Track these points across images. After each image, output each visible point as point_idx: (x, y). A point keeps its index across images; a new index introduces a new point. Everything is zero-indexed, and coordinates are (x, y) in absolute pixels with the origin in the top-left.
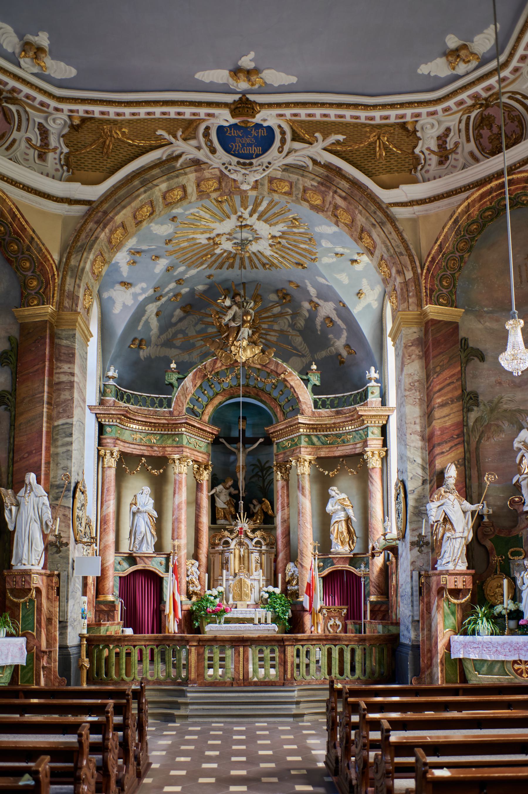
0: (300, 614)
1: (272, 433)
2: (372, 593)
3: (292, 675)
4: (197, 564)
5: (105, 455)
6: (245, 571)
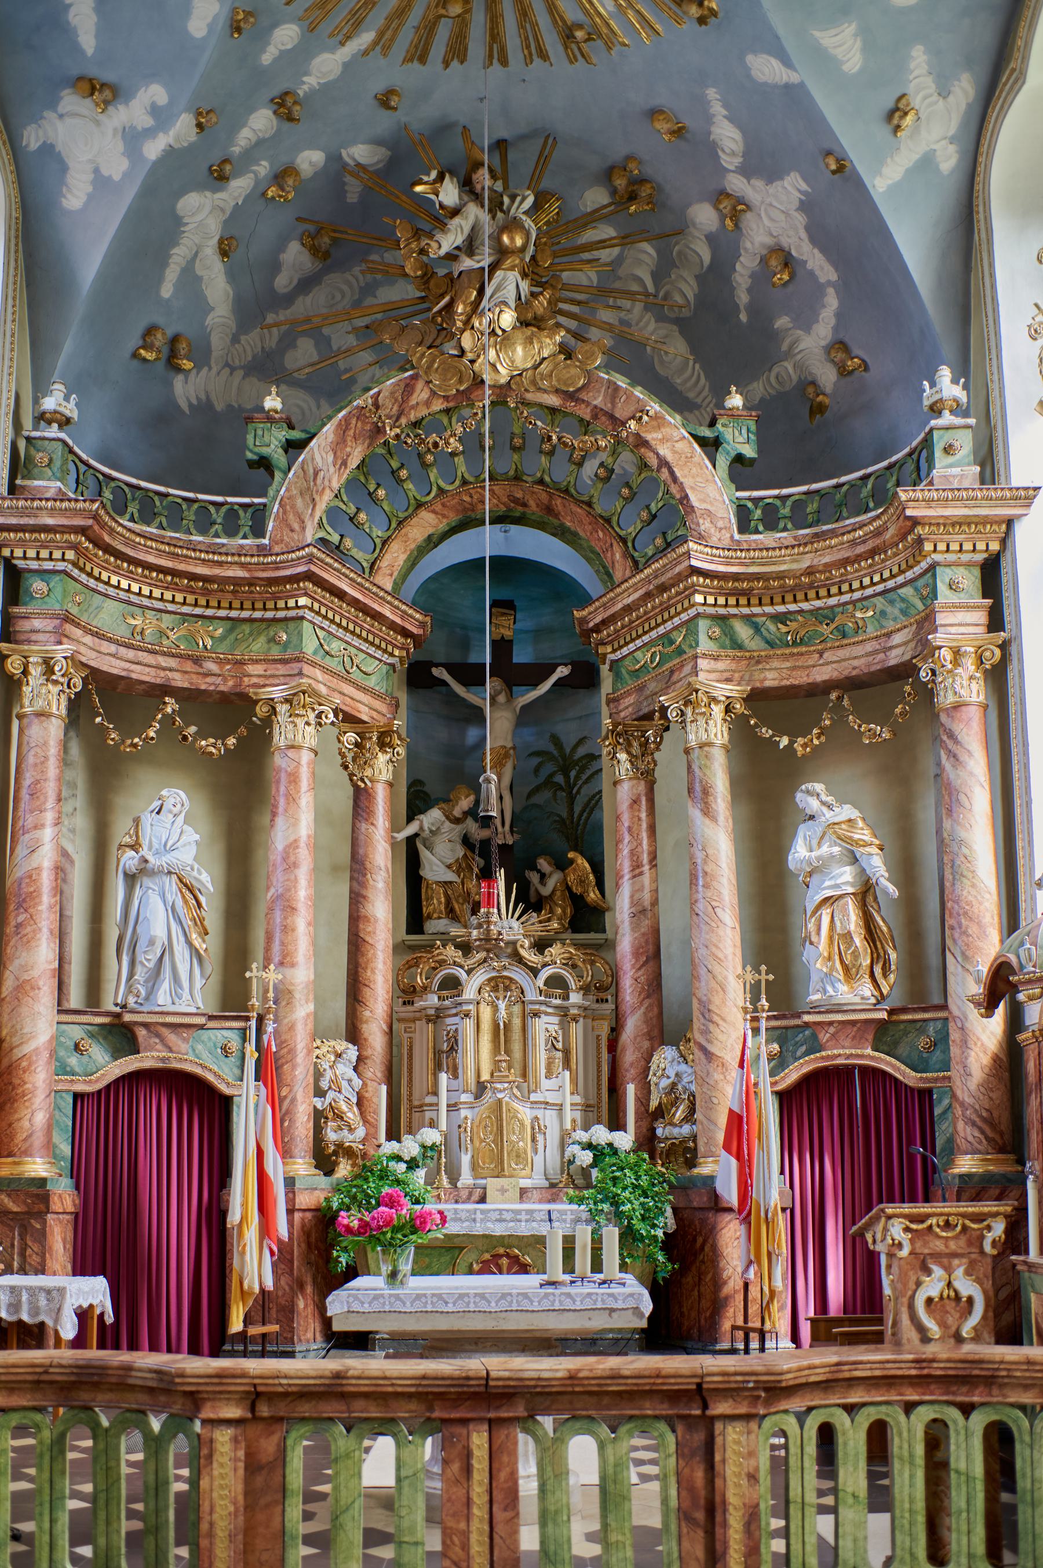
0: (703, 1221)
1: (597, 629)
2: (960, 1141)
4: (352, 1053)
5: (25, 672)
6: (514, 1075)
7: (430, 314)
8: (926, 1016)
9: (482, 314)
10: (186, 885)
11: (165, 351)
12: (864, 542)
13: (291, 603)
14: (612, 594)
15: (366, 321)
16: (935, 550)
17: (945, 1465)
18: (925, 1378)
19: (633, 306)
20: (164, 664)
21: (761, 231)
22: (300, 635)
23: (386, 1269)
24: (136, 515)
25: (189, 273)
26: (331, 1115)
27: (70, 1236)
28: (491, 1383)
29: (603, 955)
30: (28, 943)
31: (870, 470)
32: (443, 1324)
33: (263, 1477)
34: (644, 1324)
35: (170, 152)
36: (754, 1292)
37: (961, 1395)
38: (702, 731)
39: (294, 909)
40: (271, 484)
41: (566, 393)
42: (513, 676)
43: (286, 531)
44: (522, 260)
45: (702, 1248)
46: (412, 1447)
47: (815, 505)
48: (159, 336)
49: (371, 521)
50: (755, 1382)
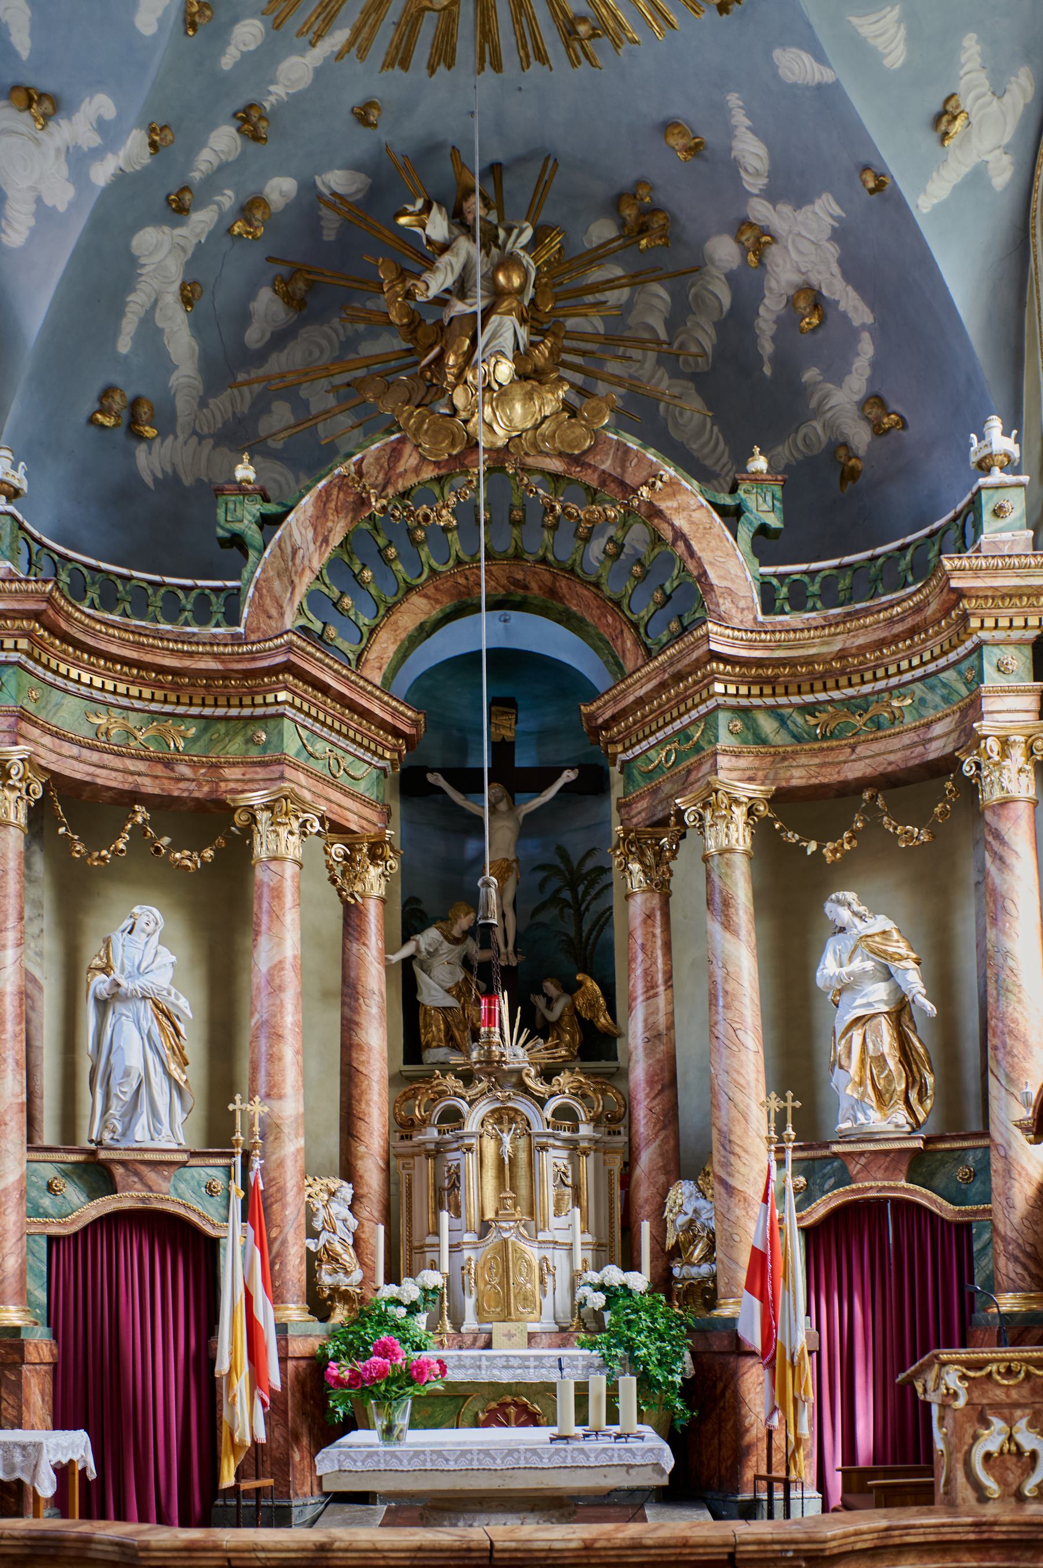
1: (607, 726)
2: (1001, 1278)
7: (418, 368)
8: (966, 1144)
9: (475, 367)
10: (162, 1011)
11: (125, 415)
12: (902, 620)
13: (270, 698)
14: (623, 686)
15: (347, 377)
16: (982, 627)
19: (645, 356)
20: (132, 768)
21: (788, 266)
22: (281, 734)
23: (380, 1423)
24: (97, 601)
25: (148, 323)
26: (325, 1257)
27: (49, 1387)
28: (496, 1555)
29: (615, 1084)
31: (909, 538)
32: (443, 1484)
34: (664, 1481)
35: (121, 177)
36: (778, 1440)
37: (1025, 1561)
38: (722, 836)
39: (280, 1036)
40: (245, 565)
41: (570, 456)
42: (515, 780)
43: (263, 618)
44: (520, 302)
45: (723, 1393)
47: (848, 581)
48: (117, 398)
49: (356, 606)
50: (794, 1551)
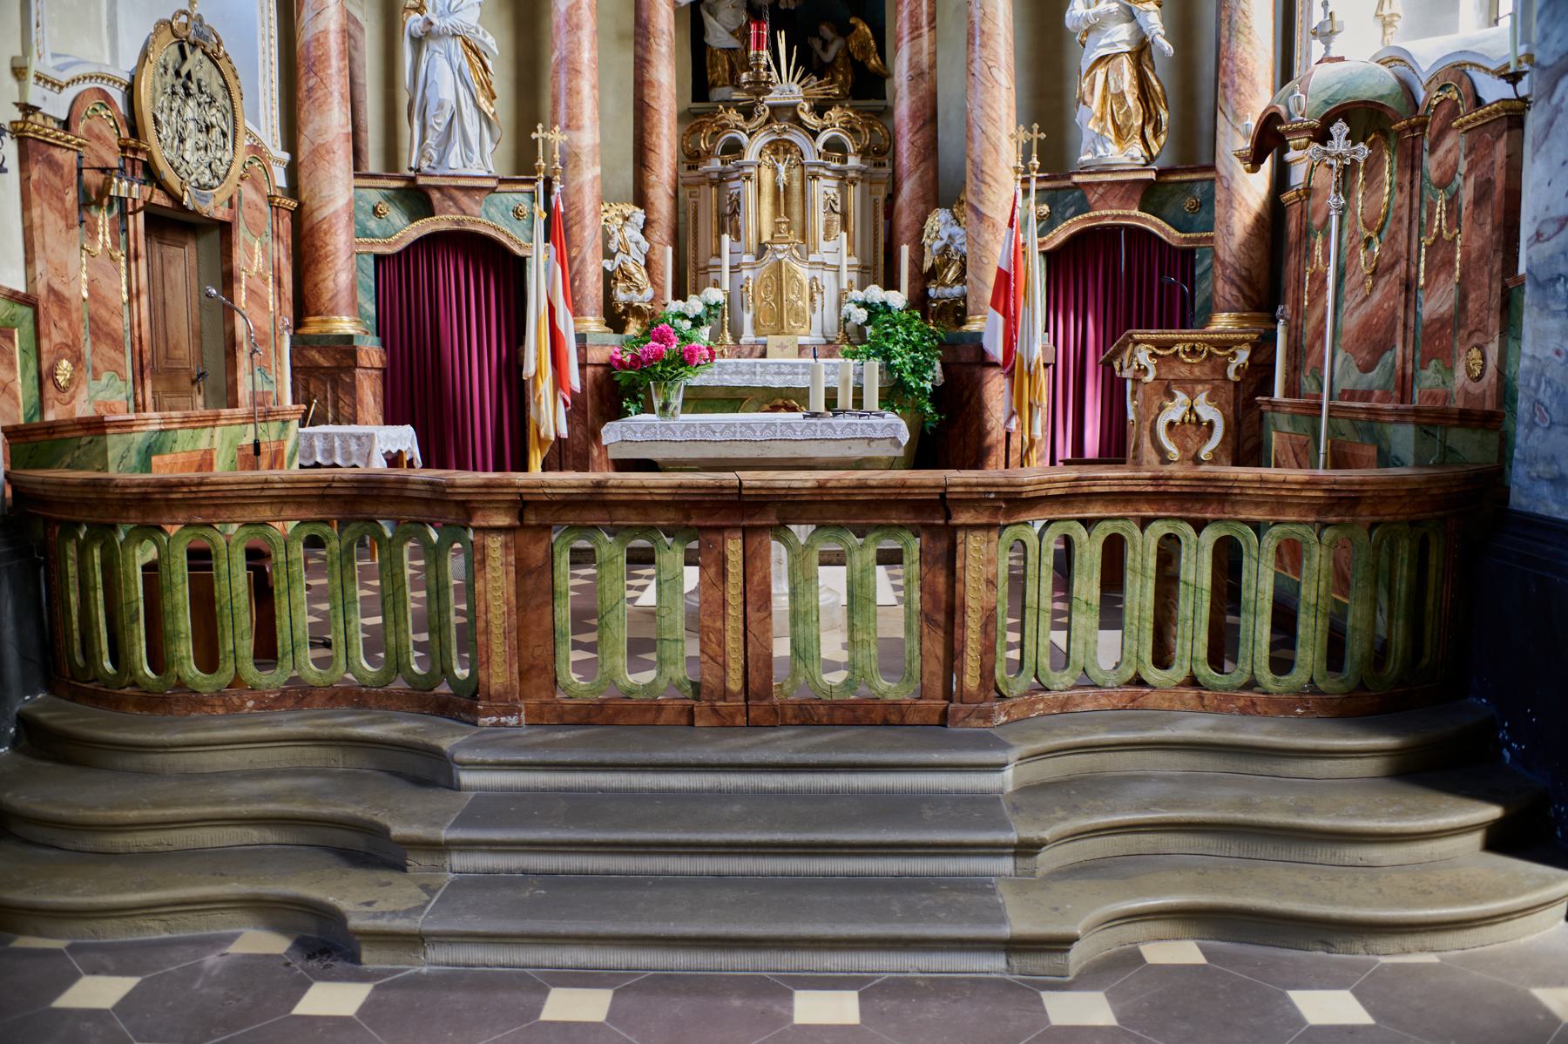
2: (1219, 300)
3: (987, 674)
4: (639, 216)
6: (793, 236)
8: (1194, 177)
17: (1175, 579)
18: (1162, 496)
26: (620, 276)
27: (379, 390)
30: (321, 107)
33: (534, 583)
36: (1015, 442)
45: (969, 401)
46: (671, 553)
